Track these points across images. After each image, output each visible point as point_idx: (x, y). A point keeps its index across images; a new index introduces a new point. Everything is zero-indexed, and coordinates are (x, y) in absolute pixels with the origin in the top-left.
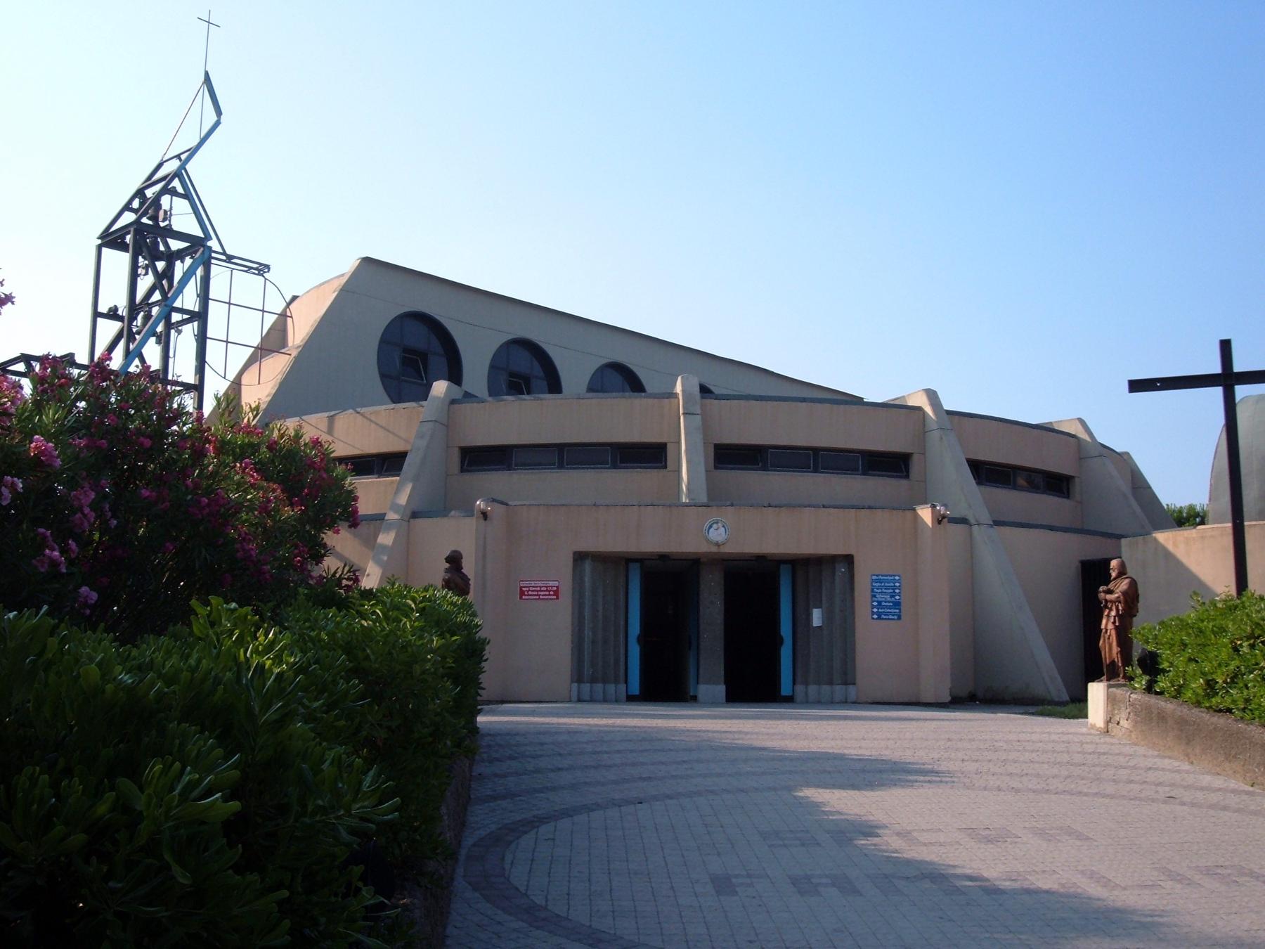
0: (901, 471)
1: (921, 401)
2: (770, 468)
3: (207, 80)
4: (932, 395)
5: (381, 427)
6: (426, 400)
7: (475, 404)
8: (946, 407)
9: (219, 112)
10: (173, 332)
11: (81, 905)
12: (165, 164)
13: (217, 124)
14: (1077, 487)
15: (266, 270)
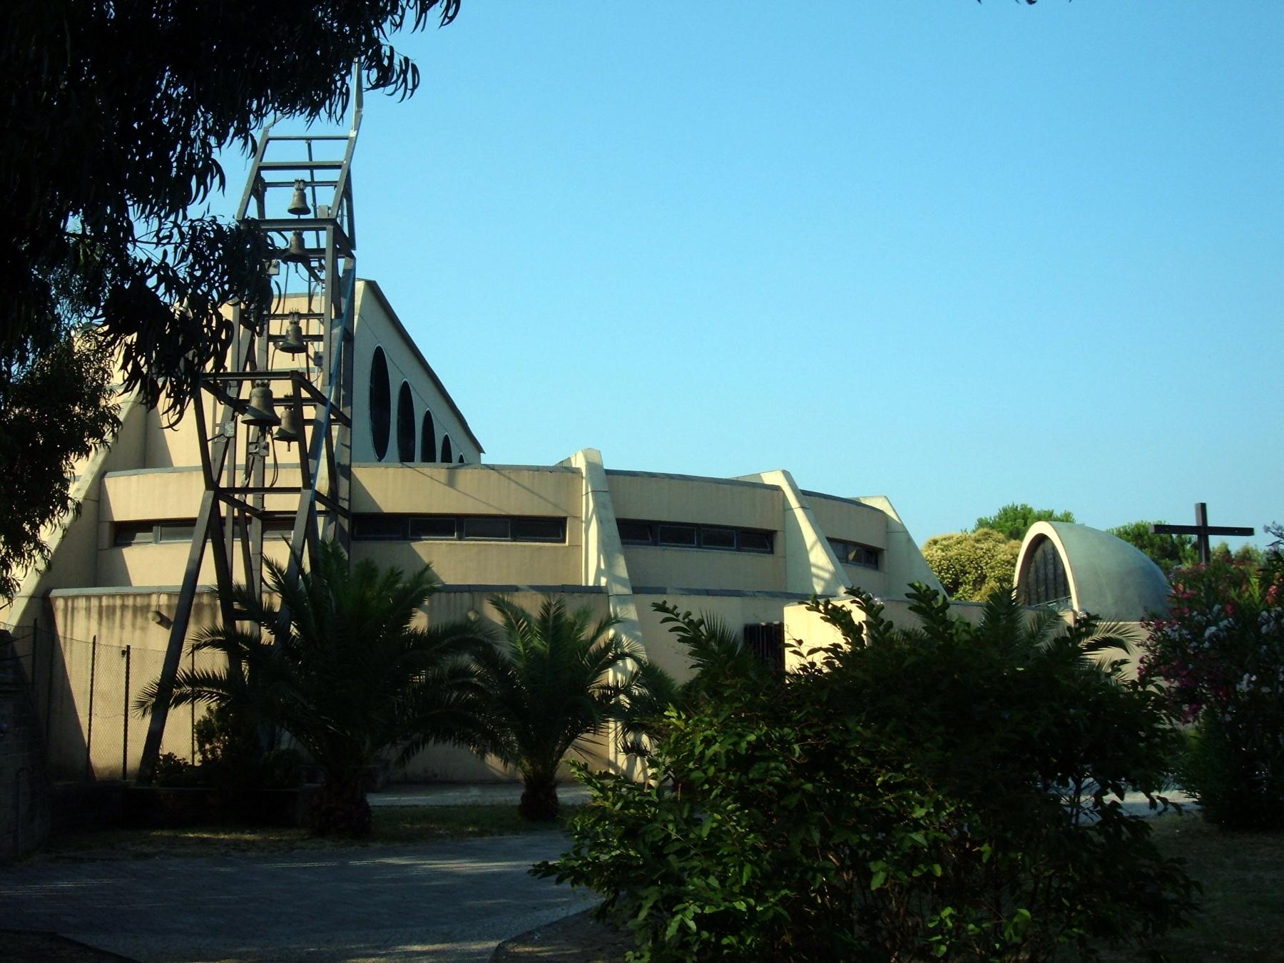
0: (765, 546)
2: (704, 546)
5: (525, 488)
10: (271, 344)
11: (140, 143)
14: (886, 558)
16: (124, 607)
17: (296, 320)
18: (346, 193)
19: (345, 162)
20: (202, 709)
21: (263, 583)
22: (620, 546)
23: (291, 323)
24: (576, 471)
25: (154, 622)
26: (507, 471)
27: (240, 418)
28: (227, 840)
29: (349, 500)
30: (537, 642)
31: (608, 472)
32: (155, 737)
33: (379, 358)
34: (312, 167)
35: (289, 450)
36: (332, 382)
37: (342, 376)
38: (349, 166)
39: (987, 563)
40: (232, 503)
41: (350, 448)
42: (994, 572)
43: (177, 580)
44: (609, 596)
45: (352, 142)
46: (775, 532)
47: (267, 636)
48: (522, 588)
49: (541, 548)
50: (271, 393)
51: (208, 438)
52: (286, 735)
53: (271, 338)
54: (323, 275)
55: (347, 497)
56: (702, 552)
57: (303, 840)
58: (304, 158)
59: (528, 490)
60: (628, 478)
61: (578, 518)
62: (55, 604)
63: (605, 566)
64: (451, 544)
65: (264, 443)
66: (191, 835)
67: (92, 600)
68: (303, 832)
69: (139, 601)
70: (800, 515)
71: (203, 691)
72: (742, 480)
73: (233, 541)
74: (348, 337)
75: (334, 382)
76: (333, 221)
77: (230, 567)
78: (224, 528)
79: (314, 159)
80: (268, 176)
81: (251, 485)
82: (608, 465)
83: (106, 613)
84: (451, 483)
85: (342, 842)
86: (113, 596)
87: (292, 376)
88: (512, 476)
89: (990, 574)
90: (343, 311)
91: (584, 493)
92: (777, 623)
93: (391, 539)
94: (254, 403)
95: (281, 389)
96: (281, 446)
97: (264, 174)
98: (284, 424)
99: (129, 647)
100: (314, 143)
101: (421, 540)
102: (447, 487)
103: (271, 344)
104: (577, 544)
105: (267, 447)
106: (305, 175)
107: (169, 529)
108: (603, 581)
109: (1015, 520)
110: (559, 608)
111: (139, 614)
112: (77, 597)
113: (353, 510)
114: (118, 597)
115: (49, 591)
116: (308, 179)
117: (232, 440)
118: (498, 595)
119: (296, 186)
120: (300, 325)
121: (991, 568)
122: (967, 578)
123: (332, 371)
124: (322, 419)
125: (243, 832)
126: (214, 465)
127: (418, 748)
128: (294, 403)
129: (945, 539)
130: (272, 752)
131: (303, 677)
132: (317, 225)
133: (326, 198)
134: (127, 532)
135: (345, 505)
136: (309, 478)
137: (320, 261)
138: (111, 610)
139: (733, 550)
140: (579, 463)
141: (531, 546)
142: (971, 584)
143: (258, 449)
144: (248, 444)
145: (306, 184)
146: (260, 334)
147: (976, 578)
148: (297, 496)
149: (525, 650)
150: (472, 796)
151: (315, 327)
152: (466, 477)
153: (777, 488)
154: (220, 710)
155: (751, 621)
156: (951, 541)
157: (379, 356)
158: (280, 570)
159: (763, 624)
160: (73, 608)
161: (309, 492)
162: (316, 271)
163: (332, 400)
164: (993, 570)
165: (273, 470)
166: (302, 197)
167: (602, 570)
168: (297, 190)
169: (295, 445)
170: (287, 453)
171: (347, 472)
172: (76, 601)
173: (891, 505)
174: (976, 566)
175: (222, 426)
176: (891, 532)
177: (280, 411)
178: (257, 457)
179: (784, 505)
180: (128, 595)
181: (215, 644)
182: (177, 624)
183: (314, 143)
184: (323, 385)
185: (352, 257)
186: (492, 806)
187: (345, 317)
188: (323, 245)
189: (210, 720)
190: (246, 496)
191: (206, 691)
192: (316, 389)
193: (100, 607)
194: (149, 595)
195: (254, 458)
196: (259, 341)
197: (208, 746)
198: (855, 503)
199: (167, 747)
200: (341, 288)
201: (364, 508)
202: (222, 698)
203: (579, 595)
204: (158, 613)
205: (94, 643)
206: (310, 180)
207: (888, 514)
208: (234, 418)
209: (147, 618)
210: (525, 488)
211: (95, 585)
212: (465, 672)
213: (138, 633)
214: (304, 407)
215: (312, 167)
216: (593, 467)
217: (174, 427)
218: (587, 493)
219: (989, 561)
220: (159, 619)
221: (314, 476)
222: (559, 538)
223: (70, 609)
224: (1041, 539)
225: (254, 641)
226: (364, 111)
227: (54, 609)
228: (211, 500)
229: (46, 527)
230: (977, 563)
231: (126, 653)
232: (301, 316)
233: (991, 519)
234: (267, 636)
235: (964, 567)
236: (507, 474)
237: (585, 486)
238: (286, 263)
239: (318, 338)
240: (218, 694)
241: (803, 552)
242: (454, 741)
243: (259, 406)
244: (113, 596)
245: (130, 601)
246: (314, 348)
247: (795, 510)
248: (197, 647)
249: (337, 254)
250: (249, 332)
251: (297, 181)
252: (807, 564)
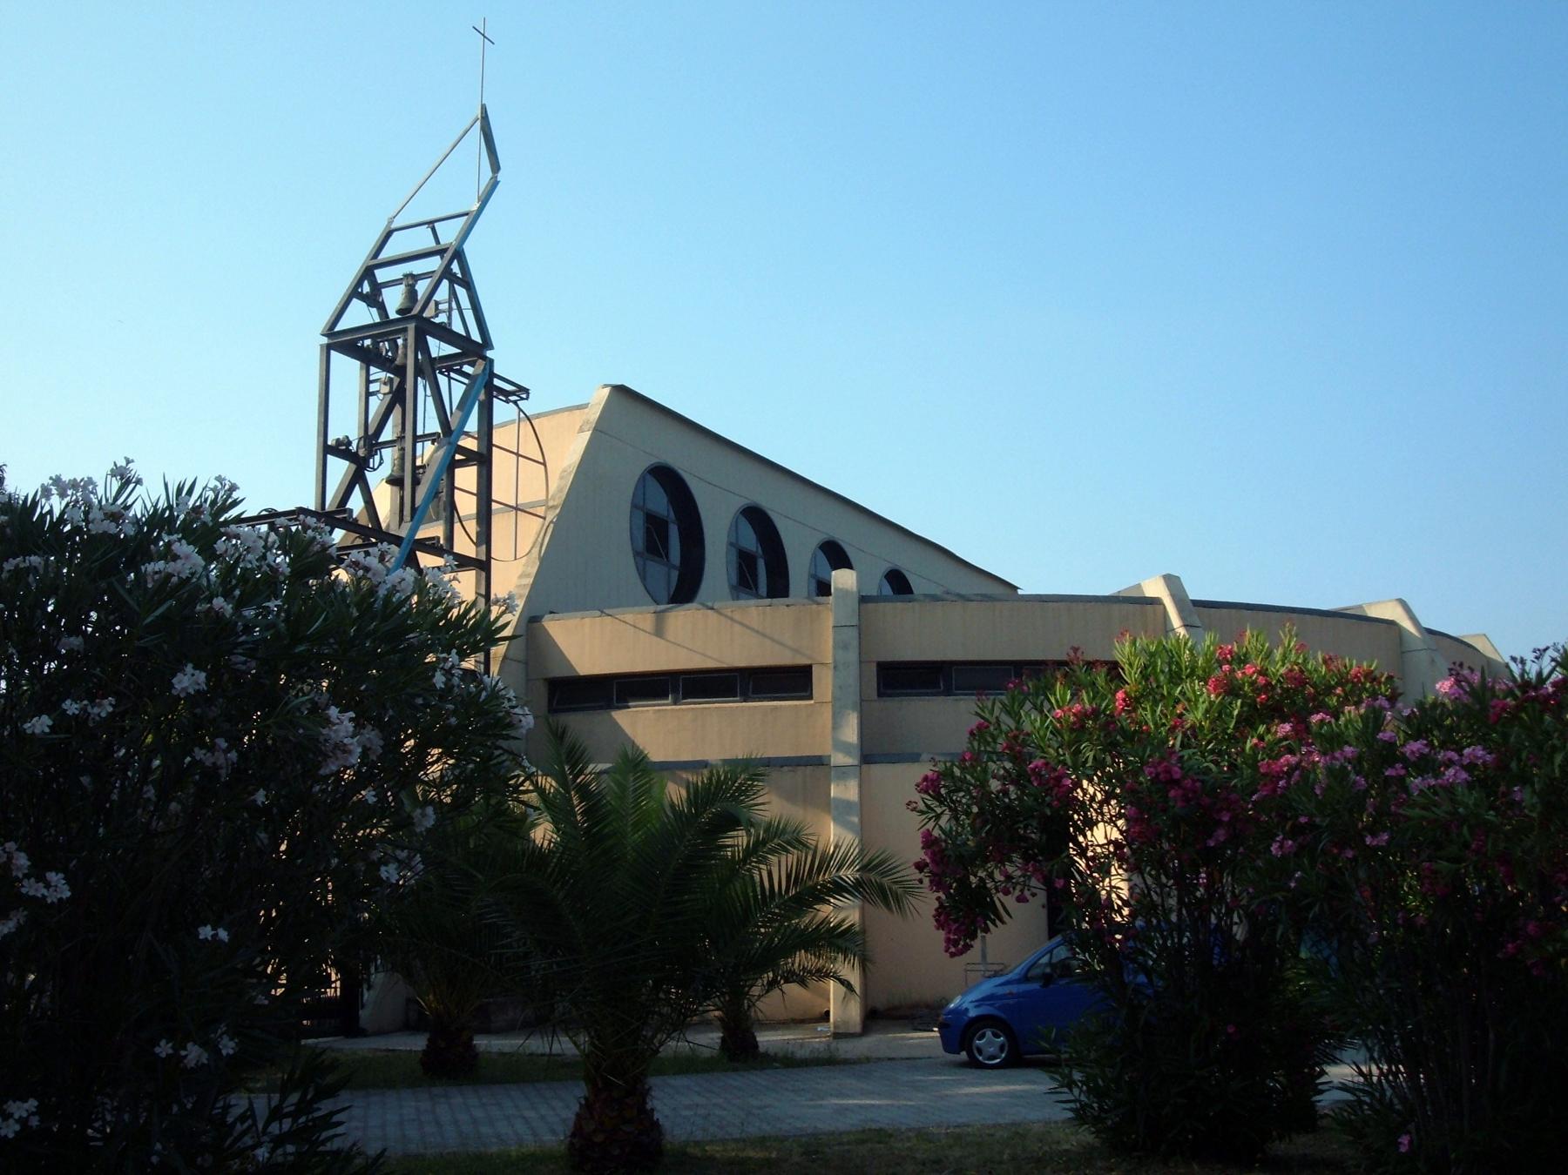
1: (1155, 588)
3: (485, 118)
4: (1172, 582)
6: (830, 594)
7: (899, 604)
8: (1192, 596)
9: (495, 166)
12: (395, 233)
13: (494, 184)
15: (524, 396)
26: (729, 610)
49: (776, 708)
58: (430, 244)
59: (757, 632)
64: (659, 710)
72: (1124, 595)
93: (594, 709)
100: (437, 225)
101: (629, 707)
102: (654, 638)
183: (437, 225)
203: (790, 768)
222: (616, 681)
236: (729, 614)
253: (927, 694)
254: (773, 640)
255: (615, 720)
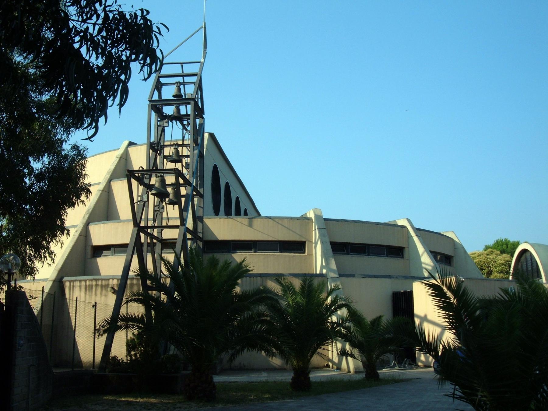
5: (286, 227)
10: (165, 160)
16: (96, 285)
17: (177, 147)
18: (200, 87)
19: (199, 73)
20: (132, 333)
21: (162, 274)
22: (332, 254)
23: (174, 149)
24: (310, 219)
25: (111, 293)
26: (277, 220)
27: (150, 193)
28: (141, 402)
29: (203, 233)
30: (299, 299)
31: (325, 219)
32: (108, 347)
33: (215, 169)
34: (183, 76)
35: (174, 209)
36: (194, 176)
37: (199, 173)
38: (201, 75)
39: (493, 265)
40: (147, 234)
41: (203, 208)
42: (496, 269)
43: (119, 272)
44: (328, 278)
45: (202, 64)
46: (404, 248)
47: (163, 297)
48: (286, 275)
49: (294, 256)
50: (165, 180)
51: (135, 202)
52: (172, 347)
53: (165, 157)
54: (189, 128)
55: (202, 232)
56: (370, 257)
57: (180, 403)
58: (180, 72)
59: (287, 228)
60: (334, 222)
61: (311, 242)
62: (65, 284)
63: (325, 264)
65: (162, 206)
66: (123, 399)
67: (82, 282)
68: (181, 397)
69: (104, 282)
70: (416, 239)
71: (129, 324)
73: (147, 254)
74: (201, 155)
75: (195, 175)
76: (194, 99)
77: (145, 267)
78: (143, 248)
79: (184, 72)
80: (163, 80)
81: (156, 225)
82: (325, 216)
83: (89, 288)
84: (250, 225)
85: (202, 404)
86: (92, 280)
87: (175, 170)
88: (280, 222)
89: (494, 270)
90: (199, 143)
91: (314, 229)
92: (409, 290)
93: (222, 252)
94: (157, 185)
95: (170, 179)
96: (170, 207)
97: (161, 79)
98: (171, 196)
99: (96, 303)
100: (184, 65)
101: (237, 253)
103: (165, 160)
104: (310, 254)
105: (163, 208)
106: (180, 79)
107: (118, 249)
108: (324, 271)
109: (502, 246)
110: (310, 281)
111: (104, 288)
112: (75, 281)
113: (205, 239)
114: (94, 281)
115: (62, 278)
116: (182, 81)
117: (147, 203)
118: (278, 278)
119: (176, 85)
120: (178, 150)
121: (495, 267)
122: (484, 272)
123: (194, 171)
124: (190, 193)
125: (150, 397)
126: (138, 215)
127: (239, 354)
128: (176, 186)
129: (472, 254)
130: (165, 355)
131: (181, 317)
132: (187, 101)
133: (190, 90)
134: (99, 250)
135: (201, 235)
136: (183, 220)
137: (187, 121)
138: (91, 287)
139: (385, 257)
140: (311, 215)
141: (289, 255)
142: (486, 274)
143: (159, 209)
144: (154, 206)
145: (181, 83)
146: (160, 154)
147: (488, 272)
148: (178, 230)
149: (293, 303)
150: (263, 377)
151: (185, 151)
152: (257, 222)
153: (404, 227)
154: (139, 334)
155: (396, 290)
156: (475, 255)
157: (215, 169)
158: (169, 263)
159: (402, 291)
160: (73, 286)
161: (183, 228)
162: (186, 126)
163: (194, 184)
164: (496, 268)
165: (166, 220)
166: (179, 90)
167: (323, 266)
168: (177, 86)
169: (177, 207)
170: (173, 212)
171: (201, 219)
172: (74, 283)
173: (456, 235)
174: (488, 266)
175: (142, 196)
176: (456, 248)
177: (169, 190)
178: (159, 213)
179: (408, 234)
180: (98, 280)
181: (136, 300)
182: (120, 292)
184: (190, 177)
185: (203, 118)
186: (275, 382)
187: (200, 145)
188: (189, 113)
189: (134, 340)
190: (153, 231)
191: (130, 324)
192: (186, 178)
193: (86, 285)
194: (109, 279)
195: (157, 213)
196: (159, 157)
197: (133, 353)
198: (439, 234)
199: (113, 353)
200: (198, 132)
201: (209, 238)
202: (139, 328)
204: (113, 288)
205: (77, 300)
206: (183, 82)
207: (455, 239)
208: (147, 193)
209: (107, 291)
210: (286, 227)
211: (84, 275)
212: (260, 315)
213: (103, 297)
214: (181, 188)
215: (183, 76)
216: (318, 217)
217: (91, 139)
218: (315, 230)
219: (494, 264)
220: (113, 291)
221: (186, 220)
223: (72, 287)
224: (525, 251)
225: (157, 300)
226: (208, 50)
227: (64, 287)
228: (136, 232)
229: (53, 242)
230: (488, 265)
231: (95, 306)
232: (179, 145)
233: (491, 245)
234: (163, 297)
235: (482, 267)
236: (277, 221)
237: (314, 226)
238: (171, 121)
239: (187, 156)
240: (137, 326)
241: (418, 257)
242: (258, 350)
243: (159, 186)
244: (92, 280)
245: (99, 283)
246: (184, 160)
247: (413, 237)
248: (127, 302)
249: (196, 116)
250: (154, 153)
251: (176, 82)
252: (420, 263)
253: (340, 254)
254: (293, 231)
255: (233, 257)
